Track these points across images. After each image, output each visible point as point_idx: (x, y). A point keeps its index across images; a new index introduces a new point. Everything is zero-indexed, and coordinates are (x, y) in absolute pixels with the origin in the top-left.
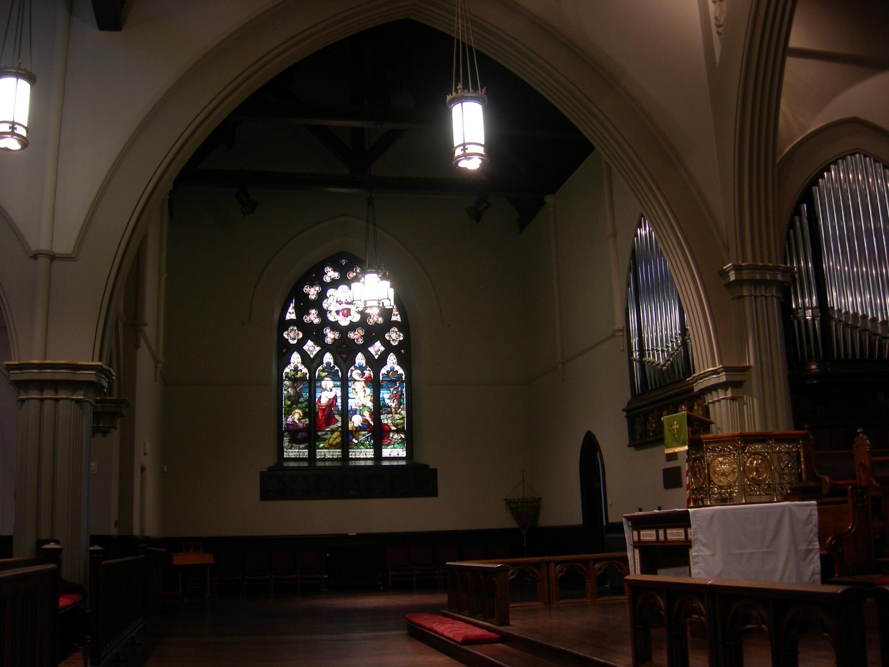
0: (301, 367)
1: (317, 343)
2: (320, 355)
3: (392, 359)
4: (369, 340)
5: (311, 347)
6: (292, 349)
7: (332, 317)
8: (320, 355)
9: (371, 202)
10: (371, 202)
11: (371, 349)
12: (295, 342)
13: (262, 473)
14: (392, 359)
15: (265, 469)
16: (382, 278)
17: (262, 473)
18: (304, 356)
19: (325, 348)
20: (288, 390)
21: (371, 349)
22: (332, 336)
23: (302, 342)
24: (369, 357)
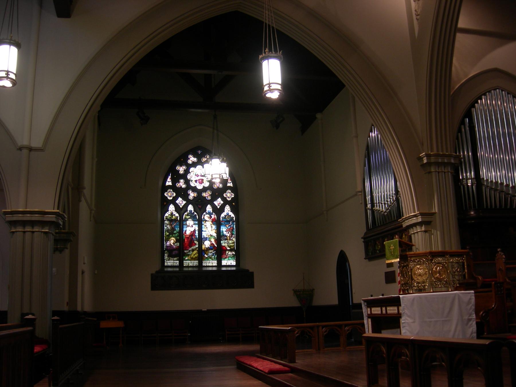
0: (175, 213)
1: (184, 199)
2: (186, 206)
3: (227, 208)
4: (214, 197)
5: (180, 201)
6: (169, 202)
7: (192, 184)
8: (186, 206)
9: (215, 117)
10: (215, 117)
11: (215, 203)
12: (171, 198)
13: (152, 275)
14: (227, 208)
15: (154, 272)
16: (222, 162)
17: (152, 275)
18: (177, 206)
19: (189, 202)
20: (167, 226)
21: (215, 203)
22: (193, 195)
23: (175, 199)
24: (214, 207)
